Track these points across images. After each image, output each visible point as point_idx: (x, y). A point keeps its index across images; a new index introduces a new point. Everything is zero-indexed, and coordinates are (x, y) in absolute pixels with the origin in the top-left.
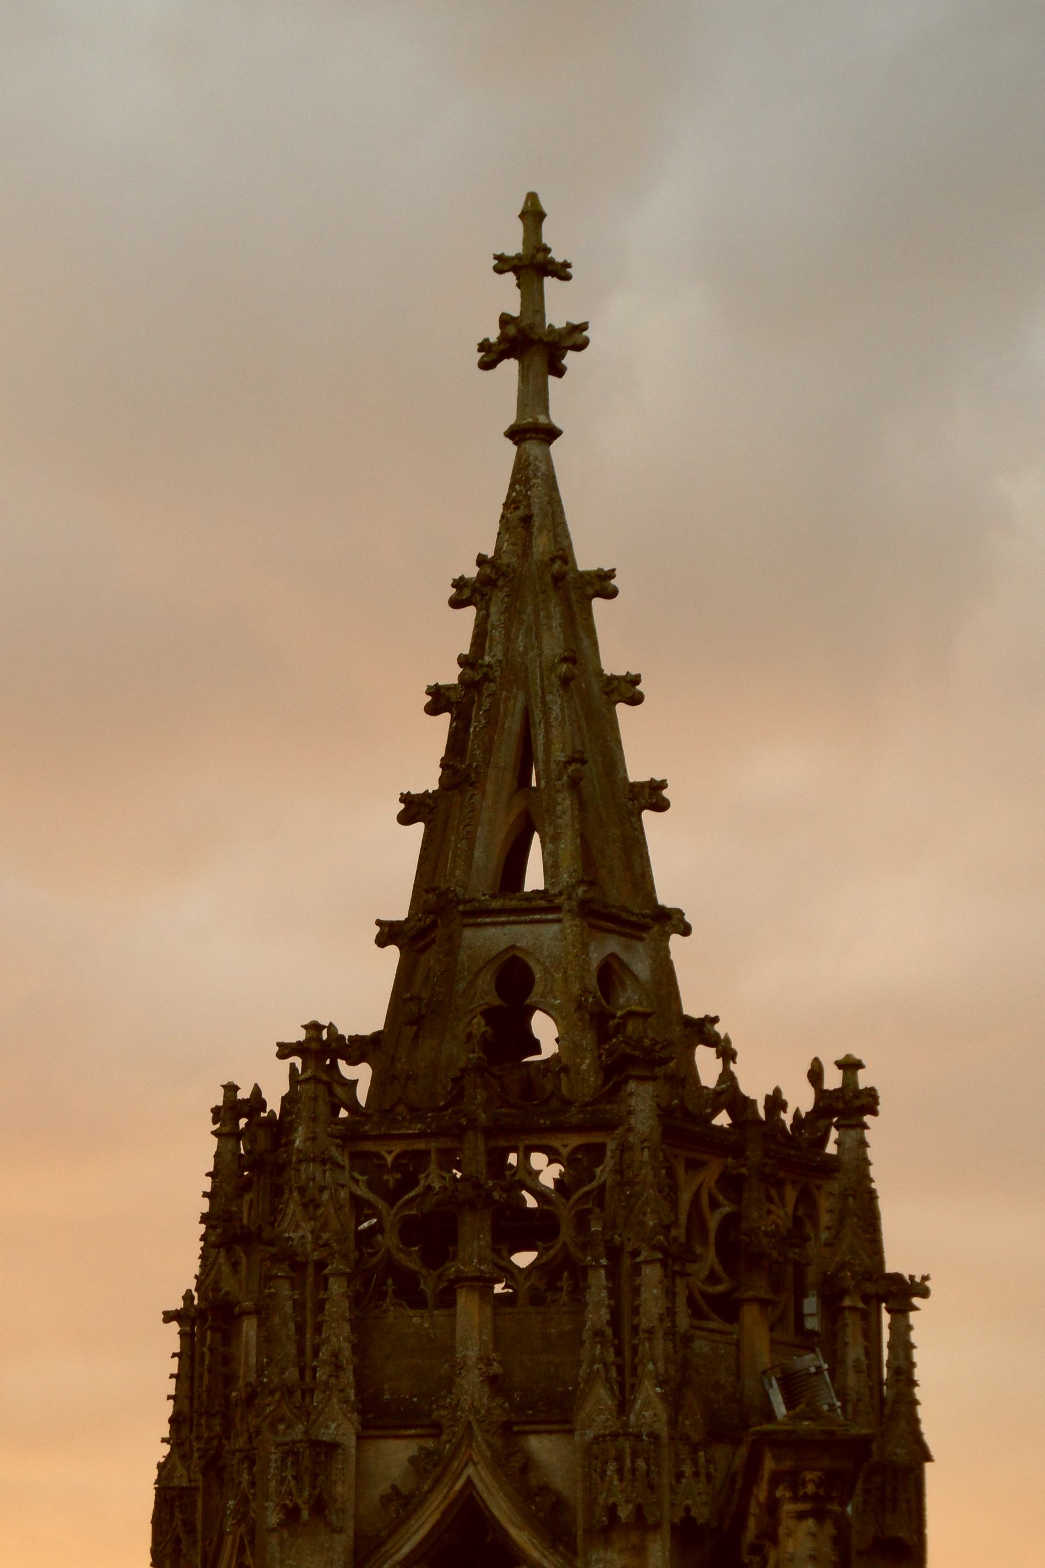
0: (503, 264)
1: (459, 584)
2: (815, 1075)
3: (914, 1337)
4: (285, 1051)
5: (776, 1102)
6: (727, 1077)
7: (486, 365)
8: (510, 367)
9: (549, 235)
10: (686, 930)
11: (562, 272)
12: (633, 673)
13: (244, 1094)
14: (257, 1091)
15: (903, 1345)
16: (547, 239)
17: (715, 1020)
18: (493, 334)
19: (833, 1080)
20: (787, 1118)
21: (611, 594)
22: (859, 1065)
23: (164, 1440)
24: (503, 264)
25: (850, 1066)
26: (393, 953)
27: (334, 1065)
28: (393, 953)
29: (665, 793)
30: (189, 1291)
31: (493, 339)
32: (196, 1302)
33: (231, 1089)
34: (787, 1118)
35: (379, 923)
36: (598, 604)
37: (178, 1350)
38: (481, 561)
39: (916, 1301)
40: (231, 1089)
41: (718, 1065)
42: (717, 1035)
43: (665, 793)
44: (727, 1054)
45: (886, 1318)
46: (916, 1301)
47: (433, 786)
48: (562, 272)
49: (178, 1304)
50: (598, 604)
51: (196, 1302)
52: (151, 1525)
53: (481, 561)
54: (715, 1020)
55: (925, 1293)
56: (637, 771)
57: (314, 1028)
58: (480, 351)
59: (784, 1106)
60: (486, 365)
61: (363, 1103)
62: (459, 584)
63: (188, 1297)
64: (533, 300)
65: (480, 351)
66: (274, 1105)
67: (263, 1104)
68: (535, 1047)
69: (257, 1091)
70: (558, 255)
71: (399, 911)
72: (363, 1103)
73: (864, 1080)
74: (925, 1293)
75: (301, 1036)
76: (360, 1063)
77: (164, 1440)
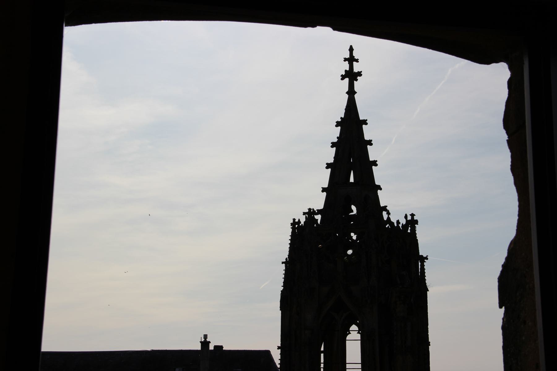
0: (345, 60)
1: (337, 122)
2: (406, 217)
3: (425, 267)
4: (304, 214)
5: (398, 222)
6: (389, 218)
7: (342, 79)
8: (347, 80)
9: (355, 54)
10: (381, 189)
11: (357, 61)
12: (371, 139)
13: (297, 221)
14: (299, 220)
15: (423, 266)
16: (354, 55)
17: (387, 206)
18: (344, 73)
19: (409, 218)
20: (400, 225)
21: (366, 124)
22: (414, 215)
23: (282, 286)
24: (345, 60)
25: (413, 215)
26: (325, 194)
27: (314, 216)
28: (325, 194)
29: (377, 163)
30: (287, 258)
31: (344, 74)
32: (288, 260)
33: (294, 220)
34: (400, 225)
35: (322, 188)
36: (364, 126)
37: (285, 269)
38: (341, 118)
39: (425, 260)
40: (294, 220)
41: (387, 216)
42: (387, 209)
43: (377, 163)
44: (388, 213)
45: (420, 264)
46: (425, 260)
47: (332, 162)
48: (357, 61)
49: (285, 261)
50: (364, 126)
51: (288, 260)
52: (288, 252)
53: (341, 118)
54: (387, 206)
55: (427, 259)
56: (371, 159)
57: (310, 209)
58: (341, 76)
59: (400, 223)
60: (342, 79)
61: (319, 223)
62: (337, 122)
63: (286, 259)
64: (351, 67)
65: (341, 76)
66: (302, 223)
67: (300, 223)
68: (352, 211)
69: (299, 220)
70: (356, 58)
71: (336, 140)
72: (319, 223)
73: (415, 218)
74: (427, 259)
75: (307, 211)
76: (345, 79)
77: (282, 286)
